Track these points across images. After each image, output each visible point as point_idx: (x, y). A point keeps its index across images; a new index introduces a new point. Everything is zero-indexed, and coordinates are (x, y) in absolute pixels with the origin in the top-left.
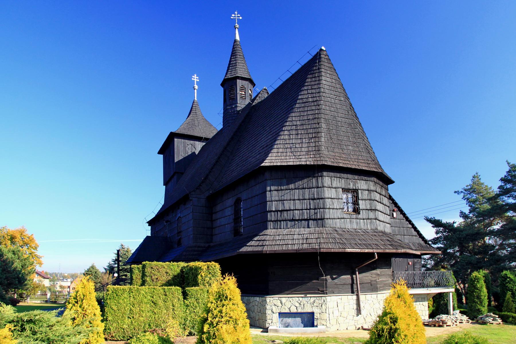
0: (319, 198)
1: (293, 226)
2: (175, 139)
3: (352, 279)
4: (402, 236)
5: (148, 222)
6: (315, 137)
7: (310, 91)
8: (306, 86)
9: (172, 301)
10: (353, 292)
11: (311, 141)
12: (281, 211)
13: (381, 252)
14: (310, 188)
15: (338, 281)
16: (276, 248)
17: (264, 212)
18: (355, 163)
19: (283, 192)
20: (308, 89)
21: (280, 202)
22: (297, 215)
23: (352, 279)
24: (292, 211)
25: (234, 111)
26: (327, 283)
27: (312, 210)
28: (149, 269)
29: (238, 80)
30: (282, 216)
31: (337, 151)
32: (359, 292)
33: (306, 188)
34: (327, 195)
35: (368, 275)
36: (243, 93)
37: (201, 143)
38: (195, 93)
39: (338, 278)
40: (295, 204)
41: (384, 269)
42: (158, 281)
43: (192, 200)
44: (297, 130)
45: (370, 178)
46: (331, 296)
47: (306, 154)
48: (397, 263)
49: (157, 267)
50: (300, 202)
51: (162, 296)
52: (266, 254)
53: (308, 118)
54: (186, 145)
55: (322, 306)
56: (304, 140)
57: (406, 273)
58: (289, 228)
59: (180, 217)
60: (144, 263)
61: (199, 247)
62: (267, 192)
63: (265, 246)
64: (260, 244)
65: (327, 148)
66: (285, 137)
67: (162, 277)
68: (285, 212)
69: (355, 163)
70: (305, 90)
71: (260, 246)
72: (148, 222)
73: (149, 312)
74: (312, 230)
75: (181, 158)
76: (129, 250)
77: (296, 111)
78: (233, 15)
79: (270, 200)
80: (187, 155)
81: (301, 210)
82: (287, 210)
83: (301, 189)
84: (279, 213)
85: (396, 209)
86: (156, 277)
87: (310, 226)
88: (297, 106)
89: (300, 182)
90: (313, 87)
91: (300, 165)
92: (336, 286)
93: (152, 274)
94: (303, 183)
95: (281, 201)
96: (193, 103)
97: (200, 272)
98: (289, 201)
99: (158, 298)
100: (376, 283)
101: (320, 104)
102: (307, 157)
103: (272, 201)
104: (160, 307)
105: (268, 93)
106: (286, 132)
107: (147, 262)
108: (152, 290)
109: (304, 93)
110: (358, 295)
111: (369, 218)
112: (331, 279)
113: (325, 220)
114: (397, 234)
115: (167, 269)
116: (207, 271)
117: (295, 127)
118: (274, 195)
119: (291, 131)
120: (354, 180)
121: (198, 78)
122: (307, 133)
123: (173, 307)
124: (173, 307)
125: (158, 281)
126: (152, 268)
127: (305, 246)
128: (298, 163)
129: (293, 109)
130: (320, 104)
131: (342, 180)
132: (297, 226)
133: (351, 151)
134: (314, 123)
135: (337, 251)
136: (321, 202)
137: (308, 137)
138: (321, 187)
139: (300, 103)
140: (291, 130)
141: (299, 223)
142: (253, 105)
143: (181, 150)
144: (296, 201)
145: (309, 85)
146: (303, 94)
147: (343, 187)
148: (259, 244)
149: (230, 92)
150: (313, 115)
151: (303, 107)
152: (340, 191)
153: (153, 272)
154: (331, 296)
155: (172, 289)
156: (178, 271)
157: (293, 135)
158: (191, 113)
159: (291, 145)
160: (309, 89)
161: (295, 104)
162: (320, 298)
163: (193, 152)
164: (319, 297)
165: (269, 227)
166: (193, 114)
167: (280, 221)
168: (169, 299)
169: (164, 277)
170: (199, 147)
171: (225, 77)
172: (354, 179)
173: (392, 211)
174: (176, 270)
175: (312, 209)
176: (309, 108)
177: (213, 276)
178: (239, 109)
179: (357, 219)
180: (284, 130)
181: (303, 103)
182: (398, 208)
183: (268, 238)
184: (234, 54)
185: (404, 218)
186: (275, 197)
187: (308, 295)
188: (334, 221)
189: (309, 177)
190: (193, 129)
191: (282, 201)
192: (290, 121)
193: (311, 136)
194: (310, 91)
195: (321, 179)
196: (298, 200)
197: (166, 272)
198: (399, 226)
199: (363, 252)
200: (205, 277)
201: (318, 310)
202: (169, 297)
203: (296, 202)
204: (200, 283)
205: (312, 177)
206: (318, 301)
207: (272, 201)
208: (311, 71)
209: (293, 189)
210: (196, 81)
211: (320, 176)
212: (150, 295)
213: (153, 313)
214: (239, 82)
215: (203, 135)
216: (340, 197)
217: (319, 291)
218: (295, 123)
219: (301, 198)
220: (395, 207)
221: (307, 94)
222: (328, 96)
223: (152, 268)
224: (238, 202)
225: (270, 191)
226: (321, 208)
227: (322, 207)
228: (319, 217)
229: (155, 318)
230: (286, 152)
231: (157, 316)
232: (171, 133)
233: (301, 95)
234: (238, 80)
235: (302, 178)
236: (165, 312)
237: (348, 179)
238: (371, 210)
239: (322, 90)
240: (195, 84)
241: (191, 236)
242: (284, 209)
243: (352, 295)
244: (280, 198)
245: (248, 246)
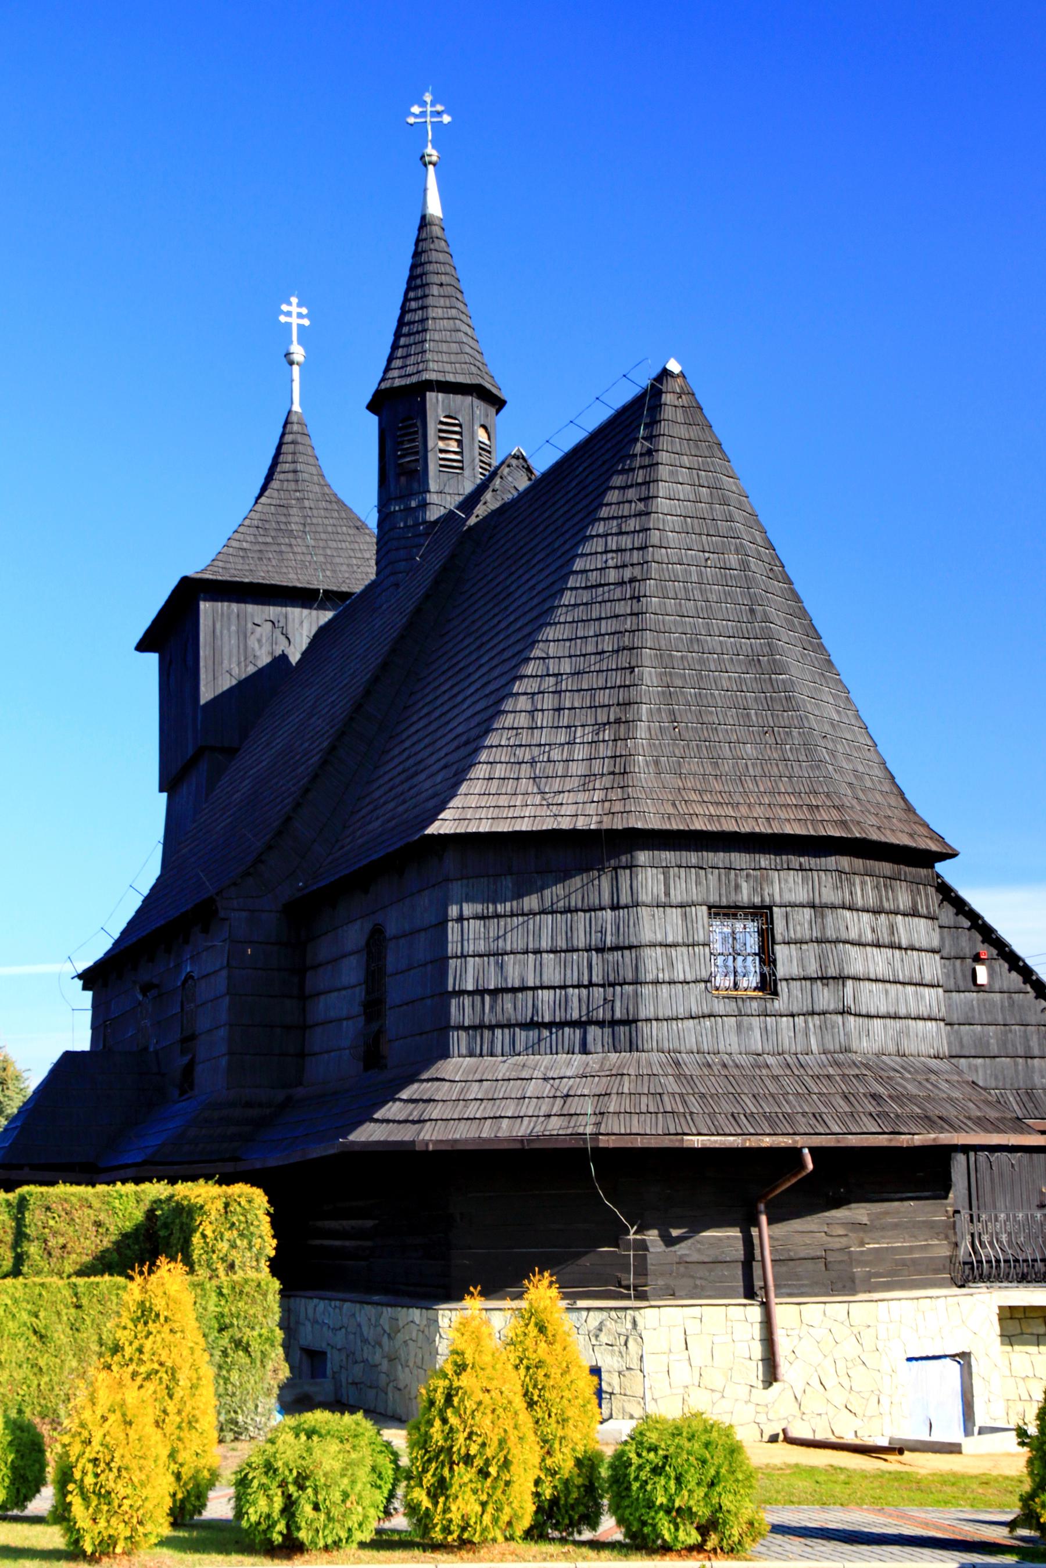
0: (621, 944)
1: (533, 1046)
2: (204, 606)
3: (748, 1243)
4: (1020, 1060)
5: (80, 976)
6: (618, 721)
7: (613, 543)
8: (604, 519)
9: (98, 1325)
10: (750, 1293)
11: (601, 739)
12: (495, 992)
13: (824, 1144)
14: (590, 910)
15: (690, 1249)
16: (487, 1131)
17: (441, 994)
18: (758, 811)
19: (502, 923)
20: (608, 535)
21: (492, 958)
22: (546, 1007)
23: (748, 1243)
24: (530, 993)
25: (417, 524)
26: (649, 1256)
27: (595, 989)
28: (37, 1212)
29: (431, 396)
30: (499, 1009)
31: (694, 768)
32: (772, 1294)
33: (577, 911)
34: (647, 934)
35: (813, 1227)
36: (453, 446)
37: (314, 612)
38: (292, 381)
39: (691, 1237)
40: (540, 968)
41: (896, 1204)
42: (65, 1255)
43: (226, 919)
44: (560, 692)
45: (823, 859)
46: (659, 1307)
47: (581, 788)
48: (1001, 1175)
49: (66, 1205)
50: (558, 960)
51: (65, 1311)
52: (426, 1153)
53: (600, 649)
54: (250, 625)
55: (626, 1344)
56: (578, 734)
57: (1015, 1217)
58: (519, 1055)
59: (189, 977)
60: (25, 1189)
61: (249, 1105)
62: (450, 924)
63: (429, 1123)
64: (415, 1113)
65: (657, 763)
66: (517, 721)
67: (82, 1240)
68: (508, 997)
69: (758, 811)
70: (598, 536)
71: (414, 1122)
72: (80, 976)
73: (20, 1366)
74: (593, 1061)
75: (226, 683)
76: (10, 1071)
77: (562, 620)
78: (416, 109)
79: (459, 954)
80: (251, 670)
81: (560, 987)
82: (514, 990)
83: (561, 913)
84: (487, 998)
85: (986, 951)
86: (61, 1241)
87: (591, 1047)
88: (568, 598)
89: (560, 886)
90: (623, 525)
91: (553, 831)
92: (682, 1269)
93: (47, 1231)
94: (567, 892)
95: (494, 955)
96: (285, 427)
97: (201, 1224)
98: (522, 956)
99: (54, 1318)
100: (846, 1258)
101: (642, 594)
102: (581, 797)
103: (463, 956)
104: (58, 1349)
105: (529, 470)
106: (523, 698)
107: (31, 1188)
108: (37, 1292)
109: (593, 551)
110: (766, 1306)
111: (817, 1009)
112: (661, 1243)
113: (640, 1024)
114: (996, 1052)
115: (100, 1210)
116: (223, 1219)
117: (552, 680)
118: (471, 936)
119: (541, 695)
120: (758, 873)
121: (304, 311)
122: (591, 707)
123: (101, 1345)
124: (101, 1345)
125: (65, 1255)
126: (48, 1209)
127: (555, 1126)
128: (548, 825)
129: (553, 608)
130: (642, 594)
131: (710, 876)
132: (548, 1045)
133: (749, 763)
134: (617, 669)
135: (653, 1146)
136: (627, 960)
137: (593, 722)
138: (627, 907)
139: (576, 588)
140: (539, 693)
141: (554, 1036)
142: (470, 528)
143: (226, 650)
144: (545, 955)
145: (613, 518)
146: (591, 554)
147: (713, 899)
148: (411, 1114)
149: (402, 443)
150: (616, 636)
151: (586, 604)
152: (699, 914)
153: (52, 1223)
154: (659, 1307)
155: (101, 1286)
156: (139, 1215)
157: (546, 713)
158: (276, 476)
159: (536, 751)
160: (611, 534)
161: (561, 591)
162: (621, 1314)
163: (278, 653)
164: (616, 1309)
165: (454, 1049)
166: (282, 476)
167: (491, 1028)
168: (88, 1322)
169: (88, 1242)
170: (305, 633)
171: (383, 380)
172: (754, 869)
173: (969, 961)
174: (130, 1213)
175: (598, 985)
176: (607, 610)
177: (242, 1235)
178: (433, 514)
179: (766, 1015)
180: (518, 694)
181: (586, 588)
182: (995, 948)
183: (442, 1091)
184: (419, 282)
185: (1028, 988)
186: (477, 942)
187: (581, 1303)
188: (675, 1027)
189: (588, 870)
190: (281, 552)
191: (498, 954)
192: (540, 658)
193: (602, 718)
194: (613, 543)
195: (628, 878)
196: (551, 951)
197: (95, 1222)
198: (1005, 1019)
199: (754, 1145)
200: (216, 1239)
201: (615, 1358)
202: (89, 1315)
203: (545, 961)
204: (199, 1261)
205: (599, 870)
206: (617, 1325)
207: (465, 957)
208: (623, 459)
209: (535, 914)
210: (299, 325)
211: (624, 868)
212: (29, 1307)
213: (36, 1370)
214: (437, 404)
215: (321, 582)
216: (701, 937)
217: (620, 1286)
218: (553, 666)
219: (561, 944)
220: (983, 942)
221: (601, 553)
222: (675, 560)
223: (48, 1209)
224: (376, 942)
225: (460, 919)
226: (625, 983)
227: (630, 977)
228: (618, 1015)
229: (39, 1385)
230: (518, 779)
231: (46, 1379)
232: (185, 582)
233: (583, 555)
234: (431, 396)
235: (564, 875)
236: (74, 1364)
237: (730, 869)
238: (822, 978)
239: (655, 537)
240: (291, 342)
241: (224, 1061)
242: (504, 986)
243: (745, 1305)
244: (493, 947)
245: (377, 1121)
